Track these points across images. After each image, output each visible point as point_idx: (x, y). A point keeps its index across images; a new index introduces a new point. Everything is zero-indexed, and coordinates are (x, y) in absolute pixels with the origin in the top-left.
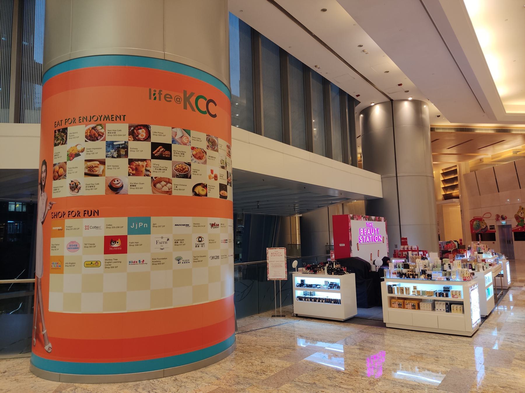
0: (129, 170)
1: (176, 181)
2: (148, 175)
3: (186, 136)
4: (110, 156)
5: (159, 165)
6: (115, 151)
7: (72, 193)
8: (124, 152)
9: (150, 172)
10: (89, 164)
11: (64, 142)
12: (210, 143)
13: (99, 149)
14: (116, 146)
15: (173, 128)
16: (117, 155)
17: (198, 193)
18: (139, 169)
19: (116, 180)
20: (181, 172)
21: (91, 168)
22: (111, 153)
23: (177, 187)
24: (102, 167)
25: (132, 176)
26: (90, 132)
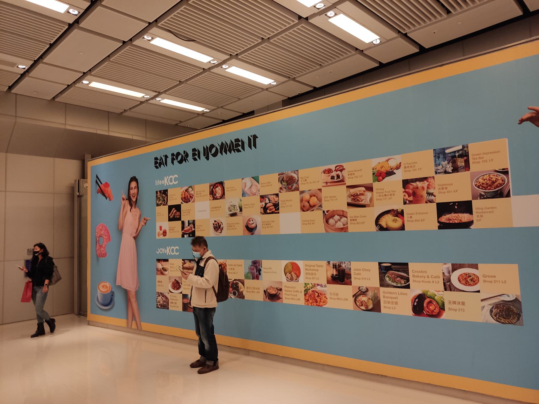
0: (405, 196)
1: (352, 212)
2: (431, 201)
3: (254, 185)
4: (442, 171)
5: (383, 189)
6: (448, 163)
7: (216, 234)
8: (462, 162)
9: (435, 196)
10: (353, 191)
11: (165, 203)
12: (283, 183)
13: (492, 153)
14: (450, 155)
15: (242, 179)
16: (452, 168)
17: (385, 226)
18: (417, 193)
19: (251, 220)
20: (489, 188)
21: (355, 197)
22: (443, 167)
23: (413, 217)
24: (369, 194)
25: (408, 204)
26: (184, 194)
